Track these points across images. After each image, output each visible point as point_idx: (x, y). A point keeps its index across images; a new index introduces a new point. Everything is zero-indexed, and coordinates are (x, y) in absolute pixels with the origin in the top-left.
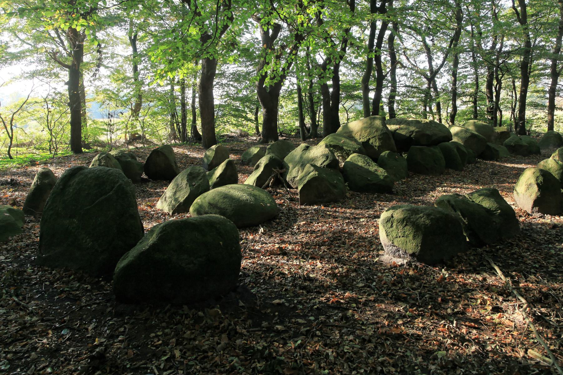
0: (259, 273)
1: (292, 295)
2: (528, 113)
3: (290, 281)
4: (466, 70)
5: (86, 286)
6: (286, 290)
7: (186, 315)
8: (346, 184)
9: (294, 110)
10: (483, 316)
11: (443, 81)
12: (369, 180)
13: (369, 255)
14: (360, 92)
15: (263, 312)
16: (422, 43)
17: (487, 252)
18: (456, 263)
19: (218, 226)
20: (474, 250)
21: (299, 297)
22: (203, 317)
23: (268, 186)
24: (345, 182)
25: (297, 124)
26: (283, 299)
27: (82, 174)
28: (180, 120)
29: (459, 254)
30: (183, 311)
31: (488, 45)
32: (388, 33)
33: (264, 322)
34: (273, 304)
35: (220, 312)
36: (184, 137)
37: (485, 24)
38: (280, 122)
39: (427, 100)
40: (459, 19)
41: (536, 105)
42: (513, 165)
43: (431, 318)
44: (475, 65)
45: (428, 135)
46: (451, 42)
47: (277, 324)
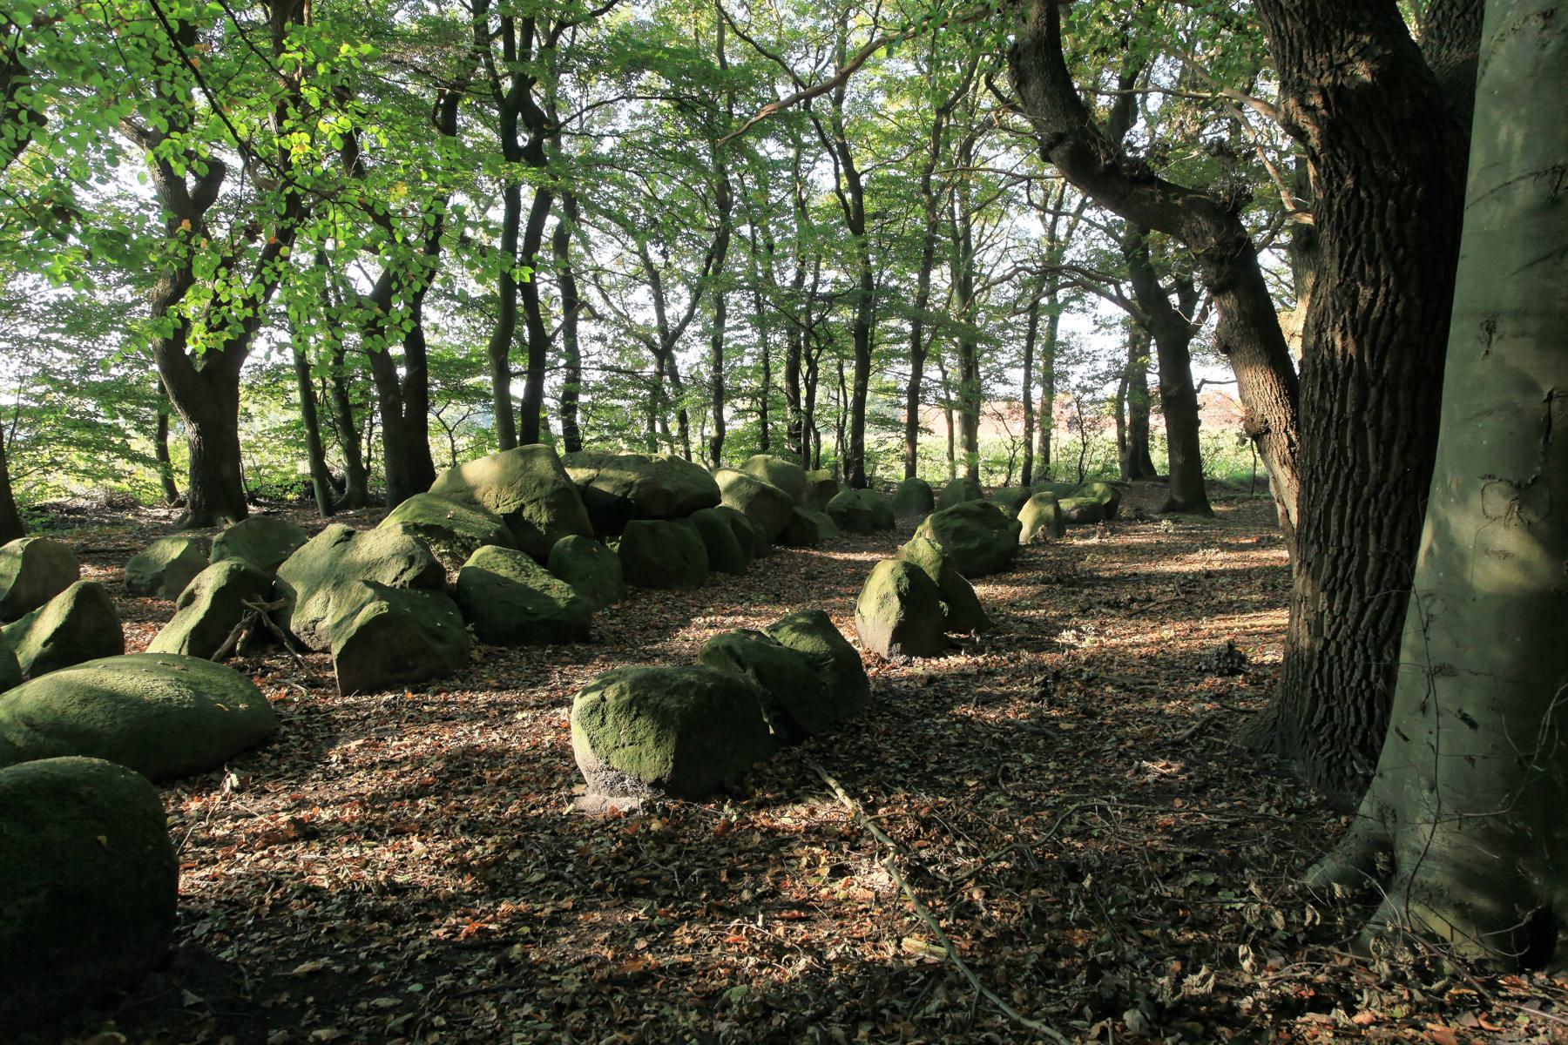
1: (349, 940)
2: (870, 439)
4: (741, 335)
8: (469, 628)
11: (691, 357)
12: (529, 613)
14: (485, 380)
17: (811, 752)
19: (84, 790)
21: (372, 940)
23: (231, 652)
25: (304, 467)
26: (322, 956)
29: (755, 766)
32: (552, 222)
34: (295, 978)
37: (781, 225)
39: (656, 404)
40: (725, 206)
41: (883, 422)
44: (761, 322)
45: (668, 493)
47: (315, 1025)
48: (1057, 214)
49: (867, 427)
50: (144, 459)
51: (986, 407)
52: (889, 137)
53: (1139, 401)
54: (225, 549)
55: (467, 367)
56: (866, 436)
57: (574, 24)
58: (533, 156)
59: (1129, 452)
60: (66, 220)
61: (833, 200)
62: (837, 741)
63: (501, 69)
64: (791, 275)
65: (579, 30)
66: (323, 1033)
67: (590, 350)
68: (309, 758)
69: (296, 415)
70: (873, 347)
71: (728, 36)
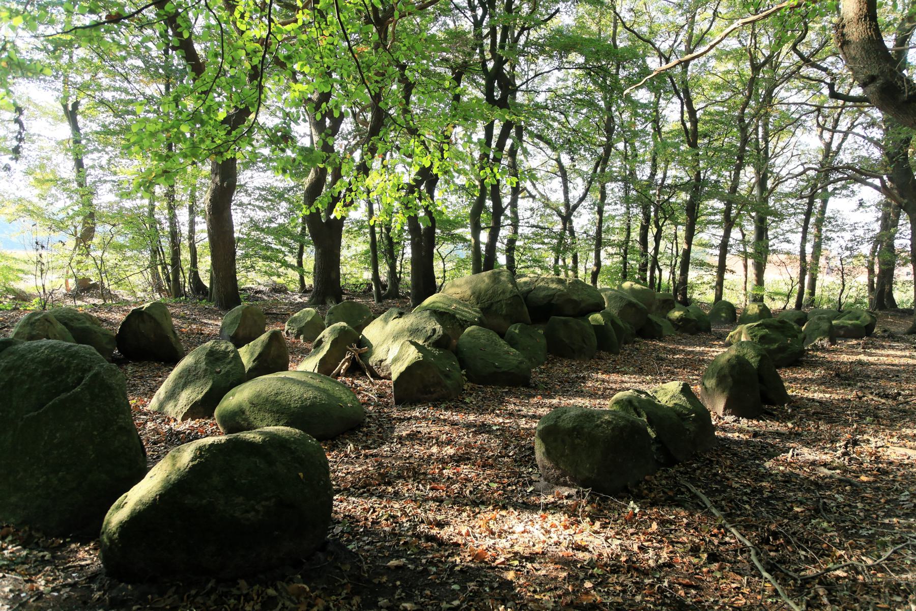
0: (353, 518)
1: (416, 550)
2: (693, 275)
3: (409, 529)
4: (614, 209)
5: (42, 554)
6: (406, 543)
7: (246, 595)
8: (463, 372)
9: (367, 252)
10: (697, 568)
11: (583, 221)
12: (496, 367)
13: (518, 482)
14: (467, 233)
15: (376, 581)
16: (554, 163)
17: (681, 473)
18: (646, 492)
19: (293, 447)
20: (664, 471)
21: (427, 553)
22: (276, 597)
23: (338, 374)
24: (462, 368)
25: (368, 275)
26: (402, 557)
27: (12, 353)
28: (168, 261)
29: (647, 477)
30: (238, 589)
31: (643, 173)
32: (509, 142)
33: (380, 599)
34: (389, 568)
35: (308, 589)
36: (177, 291)
37: (643, 143)
38: (343, 270)
39: (560, 249)
40: (609, 130)
41: (702, 264)
42: (703, 348)
43: (629, 575)
44: (626, 200)
45: (575, 301)
46: (597, 165)
47: (402, 599)
48: (834, 130)
49: (690, 266)
50: (292, 267)
51: (772, 257)
52: (718, 88)
53: (888, 257)
54: (332, 317)
55: (456, 224)
56: (690, 273)
57: (528, 29)
58: (502, 104)
59: (876, 293)
60: (287, 142)
61: (679, 126)
62: (698, 468)
63: (488, 56)
64: (648, 172)
65: (531, 32)
66: (408, 605)
67: (523, 213)
68: (382, 438)
69: (367, 247)
70: (698, 217)
71: (620, 29)
